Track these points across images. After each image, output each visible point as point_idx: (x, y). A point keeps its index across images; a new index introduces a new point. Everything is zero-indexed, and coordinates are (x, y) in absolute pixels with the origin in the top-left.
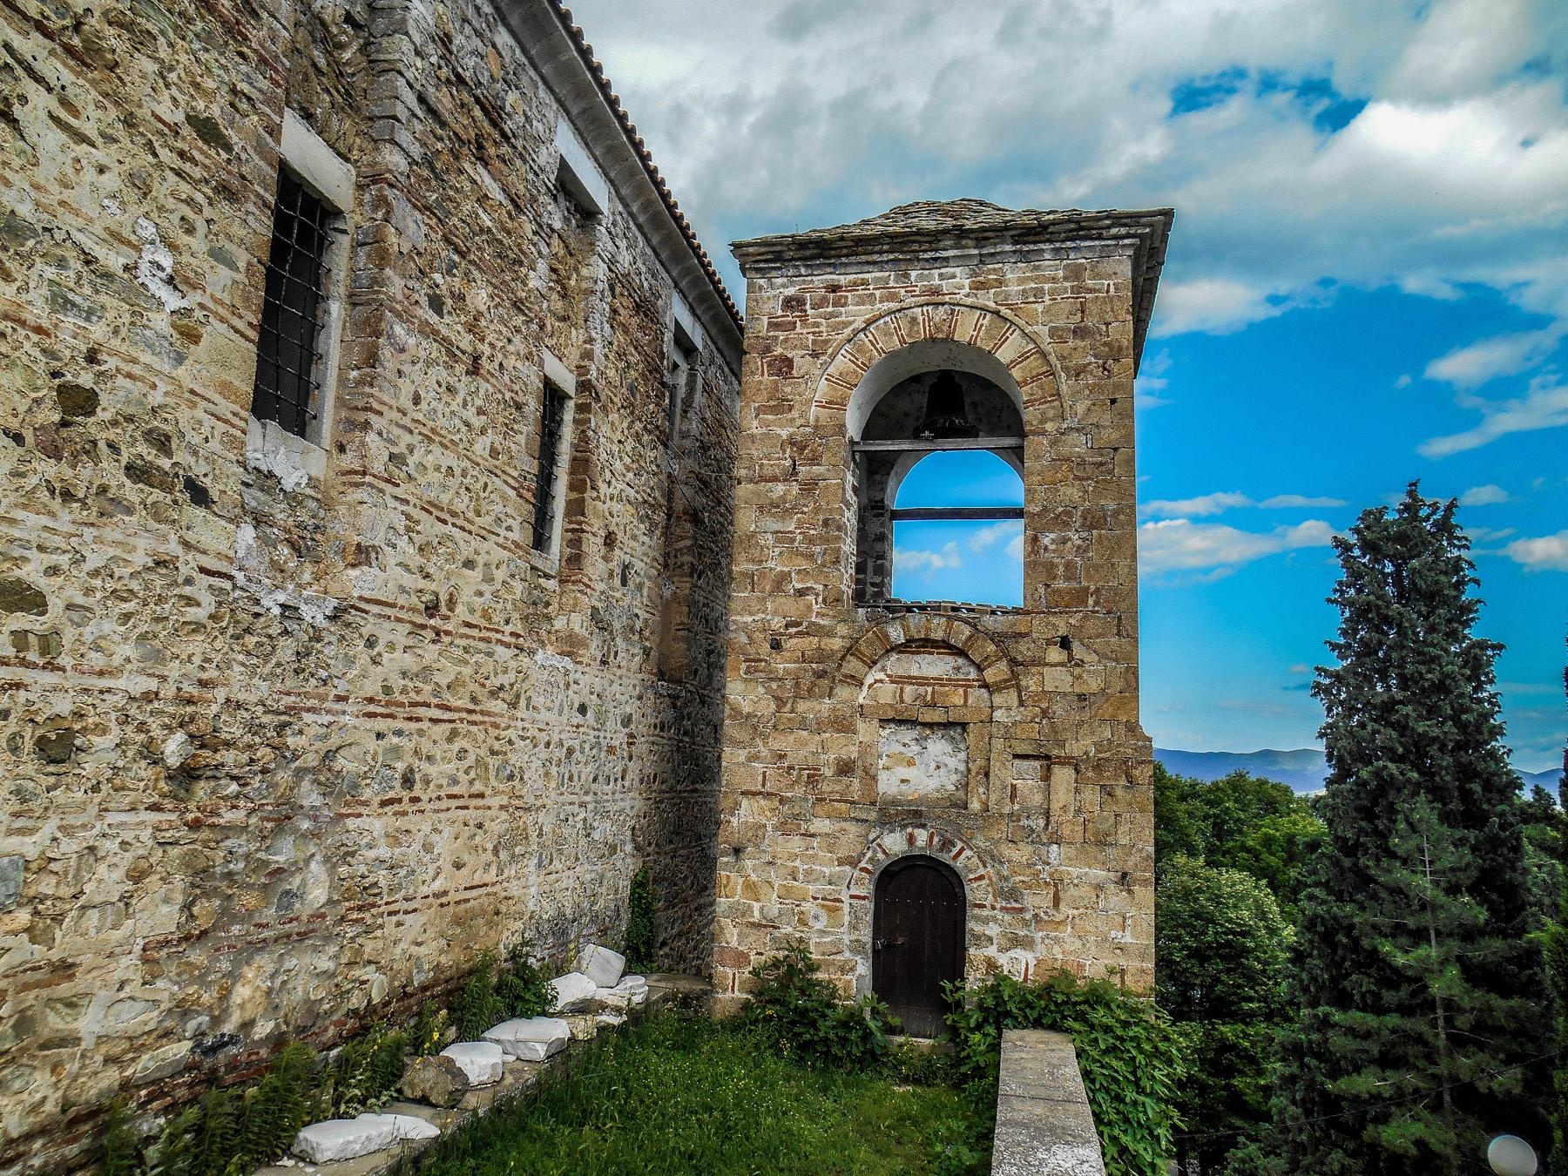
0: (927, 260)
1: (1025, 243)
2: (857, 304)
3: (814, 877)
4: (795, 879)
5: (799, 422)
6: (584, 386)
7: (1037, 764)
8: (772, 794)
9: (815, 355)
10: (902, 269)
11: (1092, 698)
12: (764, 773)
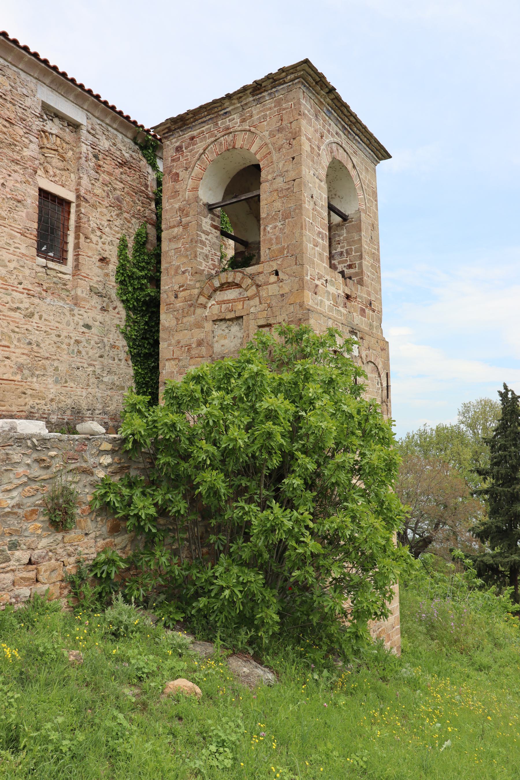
1: (257, 95)
2: (201, 142)
6: (78, 197)
10: (214, 120)
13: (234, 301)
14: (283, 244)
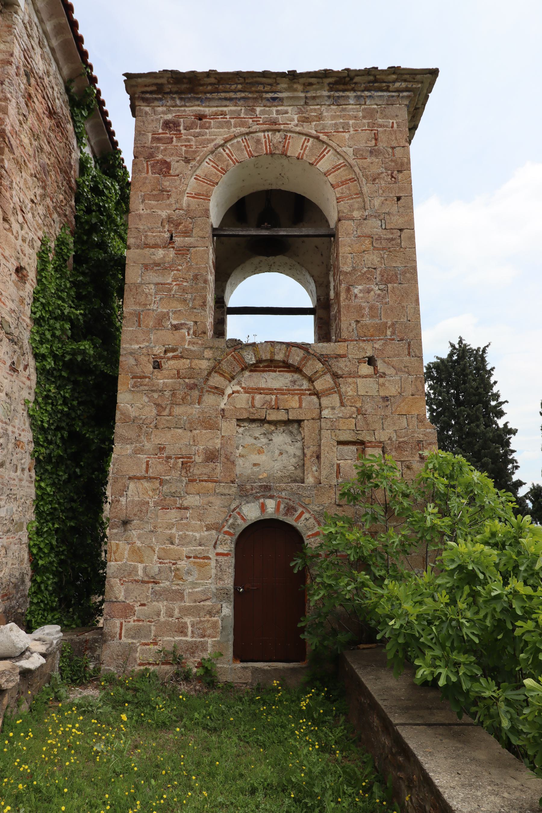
0: (268, 99)
1: (337, 90)
2: (218, 128)
3: (188, 540)
4: (172, 543)
5: (174, 207)
7: (354, 448)
8: (154, 478)
9: (187, 161)
11: (392, 399)
12: (148, 462)
13: (280, 391)
14: (384, 320)
